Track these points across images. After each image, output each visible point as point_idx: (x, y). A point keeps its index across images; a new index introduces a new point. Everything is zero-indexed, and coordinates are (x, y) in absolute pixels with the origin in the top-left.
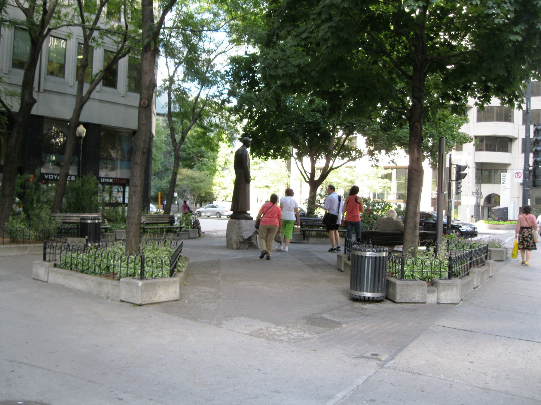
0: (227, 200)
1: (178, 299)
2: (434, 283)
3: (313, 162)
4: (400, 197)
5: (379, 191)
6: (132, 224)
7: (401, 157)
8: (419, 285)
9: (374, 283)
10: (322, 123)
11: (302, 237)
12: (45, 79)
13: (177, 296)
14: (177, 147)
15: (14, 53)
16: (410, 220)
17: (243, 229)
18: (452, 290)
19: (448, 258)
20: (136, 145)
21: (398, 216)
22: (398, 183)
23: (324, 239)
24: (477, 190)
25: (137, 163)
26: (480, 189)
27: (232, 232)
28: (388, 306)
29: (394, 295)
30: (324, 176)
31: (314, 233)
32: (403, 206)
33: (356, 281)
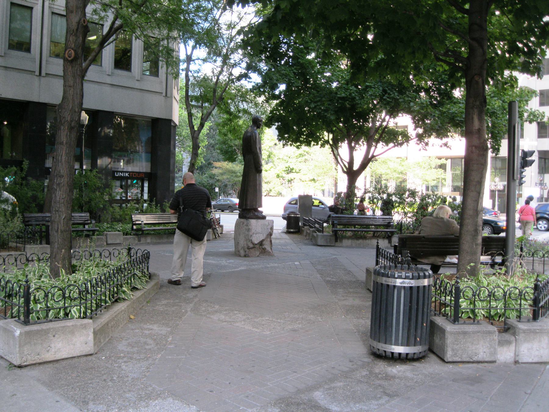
0: (270, 194)
1: (92, 352)
2: (509, 329)
3: (352, 149)
4: (455, 189)
5: (433, 183)
6: (57, 231)
7: (457, 145)
8: (484, 332)
9: (409, 330)
10: (357, 98)
11: (334, 238)
12: (47, 61)
13: (89, 348)
14: (195, 135)
15: (11, 31)
16: (468, 221)
17: (253, 231)
18: (540, 341)
19: (532, 285)
20: (60, 116)
21: (453, 211)
22: (453, 174)
23: (360, 241)
24: (541, 181)
25: (62, 143)
26: (543, 180)
27: (240, 234)
28: (431, 370)
29: (443, 348)
30: (364, 166)
31: (349, 234)
32: (459, 199)
33: (380, 326)
